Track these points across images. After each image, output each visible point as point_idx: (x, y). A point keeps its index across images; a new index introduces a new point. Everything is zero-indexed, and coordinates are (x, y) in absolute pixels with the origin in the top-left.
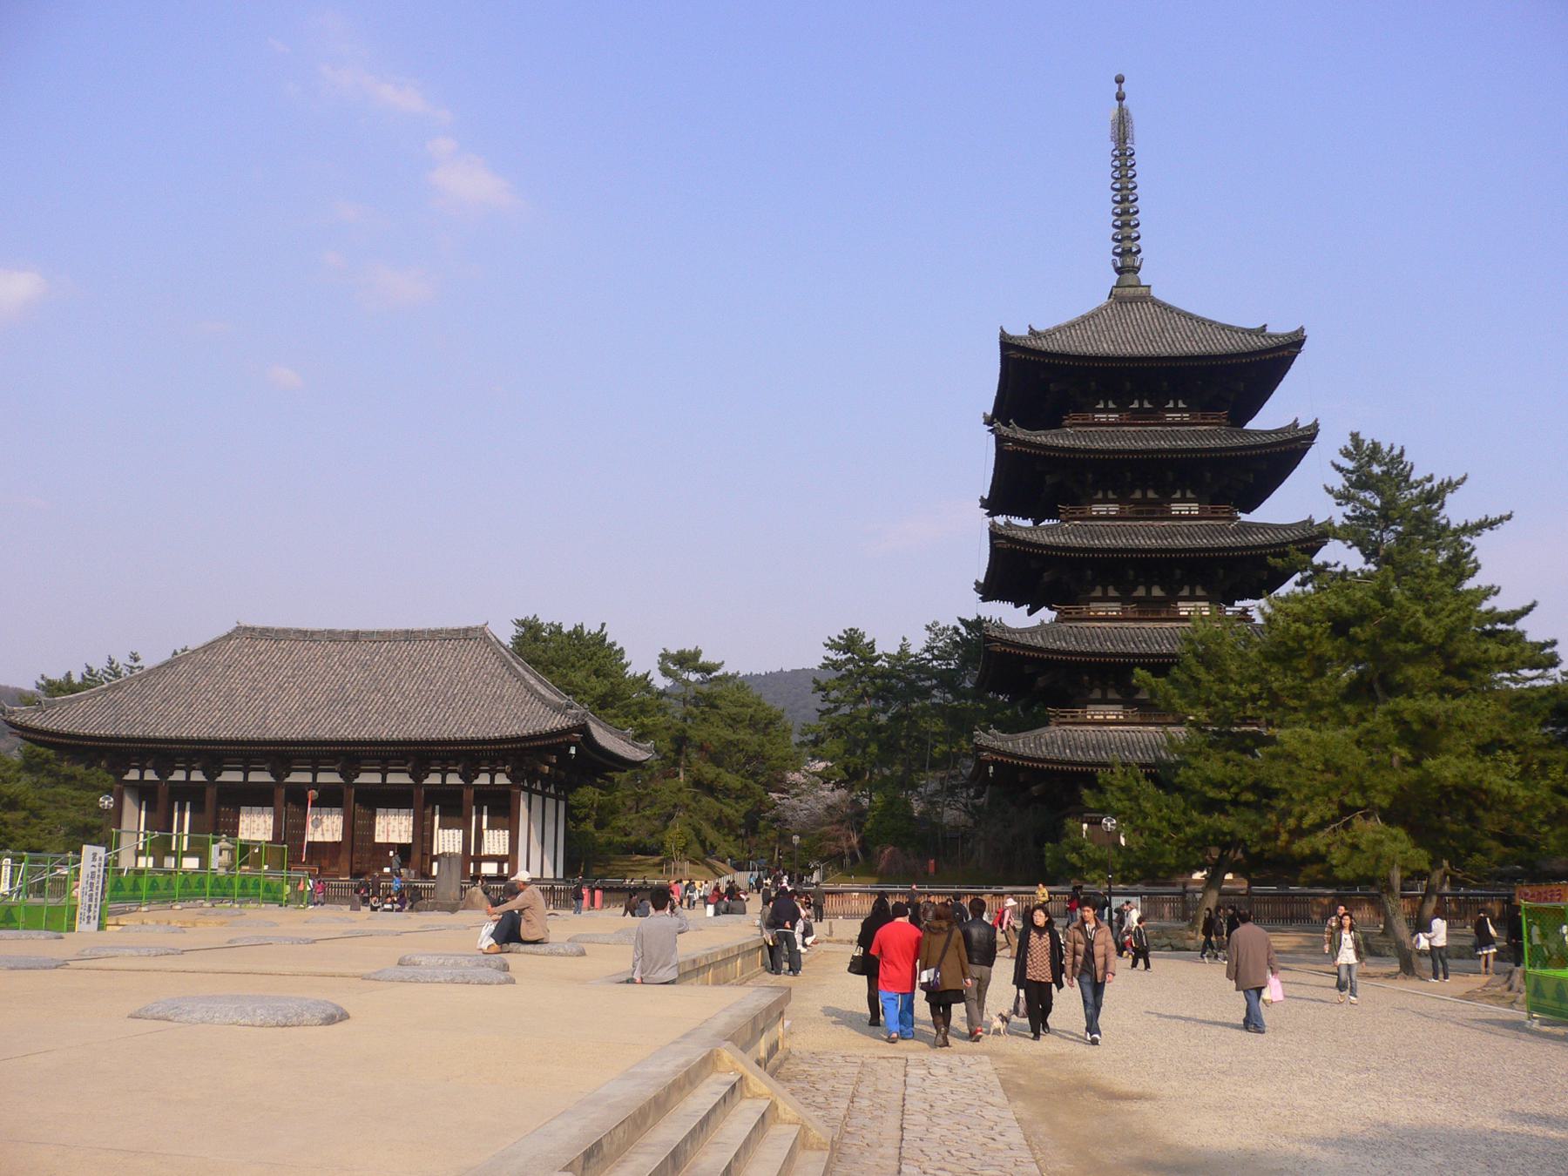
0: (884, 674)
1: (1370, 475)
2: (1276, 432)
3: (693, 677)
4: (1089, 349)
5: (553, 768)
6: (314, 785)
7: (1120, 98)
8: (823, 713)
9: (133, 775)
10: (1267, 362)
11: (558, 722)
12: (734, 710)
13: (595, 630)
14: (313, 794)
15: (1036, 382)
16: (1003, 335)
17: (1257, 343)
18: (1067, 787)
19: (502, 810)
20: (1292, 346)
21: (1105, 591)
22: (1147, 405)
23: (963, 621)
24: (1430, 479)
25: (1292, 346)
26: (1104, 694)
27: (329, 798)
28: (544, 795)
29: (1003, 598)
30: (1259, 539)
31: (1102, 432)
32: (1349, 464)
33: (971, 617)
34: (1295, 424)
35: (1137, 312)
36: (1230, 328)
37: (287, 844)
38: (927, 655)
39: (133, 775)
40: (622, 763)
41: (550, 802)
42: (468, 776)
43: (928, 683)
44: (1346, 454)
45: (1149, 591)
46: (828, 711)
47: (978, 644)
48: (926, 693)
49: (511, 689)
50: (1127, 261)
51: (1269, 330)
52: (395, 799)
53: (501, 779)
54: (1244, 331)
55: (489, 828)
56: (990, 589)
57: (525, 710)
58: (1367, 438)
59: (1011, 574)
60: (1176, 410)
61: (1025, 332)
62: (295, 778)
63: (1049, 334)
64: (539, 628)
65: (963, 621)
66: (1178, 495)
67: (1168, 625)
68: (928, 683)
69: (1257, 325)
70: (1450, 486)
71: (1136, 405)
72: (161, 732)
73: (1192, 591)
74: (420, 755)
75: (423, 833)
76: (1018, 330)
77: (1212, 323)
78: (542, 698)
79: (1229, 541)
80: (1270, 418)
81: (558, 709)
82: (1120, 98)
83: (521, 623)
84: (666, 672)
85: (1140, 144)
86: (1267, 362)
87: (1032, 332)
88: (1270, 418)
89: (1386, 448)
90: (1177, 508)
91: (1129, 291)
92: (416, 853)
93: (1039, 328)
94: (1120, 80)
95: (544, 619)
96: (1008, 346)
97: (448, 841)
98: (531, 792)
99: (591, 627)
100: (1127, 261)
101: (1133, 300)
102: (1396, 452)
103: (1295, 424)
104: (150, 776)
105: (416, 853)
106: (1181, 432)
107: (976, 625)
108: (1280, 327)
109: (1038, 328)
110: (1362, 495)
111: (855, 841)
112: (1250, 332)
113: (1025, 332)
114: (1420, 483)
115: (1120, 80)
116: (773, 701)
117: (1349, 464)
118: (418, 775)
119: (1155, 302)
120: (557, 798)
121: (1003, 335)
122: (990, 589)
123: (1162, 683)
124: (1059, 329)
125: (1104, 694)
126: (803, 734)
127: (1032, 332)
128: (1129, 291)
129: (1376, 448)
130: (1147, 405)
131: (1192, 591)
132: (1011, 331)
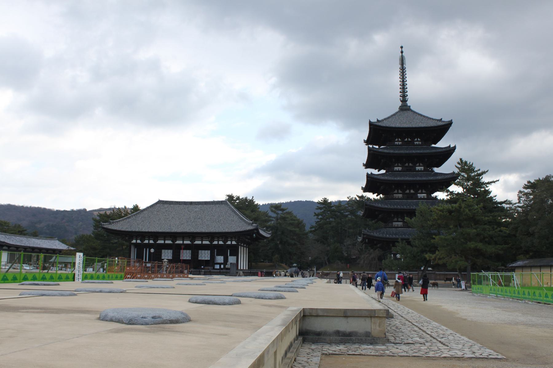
0: (334, 211)
1: (464, 169)
2: (445, 148)
3: (280, 212)
4: (393, 125)
5: (248, 238)
6: (183, 244)
7: (402, 52)
8: (317, 222)
9: (134, 241)
10: (442, 129)
11: (250, 228)
12: (291, 222)
13: (251, 198)
14: (183, 247)
15: (378, 134)
16: (370, 121)
17: (440, 124)
18: (387, 245)
19: (235, 252)
20: (450, 124)
21: (398, 191)
22: (409, 140)
23: (357, 196)
24: (479, 170)
25: (450, 124)
26: (398, 219)
27: (187, 247)
28: (244, 247)
29: (369, 191)
30: (440, 178)
31: (398, 147)
32: (459, 166)
33: (360, 195)
34: (450, 146)
35: (406, 113)
36: (432, 119)
37: (176, 259)
38: (347, 206)
39: (134, 241)
40: (265, 237)
41: (245, 248)
42: (225, 242)
43: (347, 213)
44: (459, 163)
45: (410, 191)
46: (318, 222)
47: (361, 203)
48: (347, 216)
49: (236, 218)
50: (404, 98)
51: (443, 120)
52: (204, 247)
53: (234, 243)
54: (436, 120)
55: (230, 255)
56: (365, 190)
57: (239, 224)
58: (464, 160)
59: (372, 184)
60: (417, 141)
61: (376, 121)
62: (178, 242)
63: (382, 120)
64: (233, 197)
65: (357, 196)
66: (418, 165)
67: (415, 201)
68: (347, 213)
69: (439, 118)
70: (484, 173)
71: (406, 140)
72: (143, 230)
73: (422, 191)
74: (211, 236)
75: (213, 257)
76: (374, 120)
77: (427, 117)
78: (244, 221)
79: (432, 178)
80: (442, 144)
81: (249, 224)
82: (402, 52)
83: (228, 196)
84: (272, 211)
85: (406, 66)
86: (442, 129)
87: (378, 120)
88: (442, 144)
89: (468, 163)
90: (417, 168)
91: (405, 107)
92: (211, 263)
93: (379, 119)
94: (402, 47)
95: (235, 194)
96: (371, 124)
97: (220, 259)
98: (241, 246)
99: (250, 198)
100: (404, 98)
101: (406, 110)
102: (471, 164)
103: (450, 146)
104: (139, 241)
105: (211, 263)
106: (417, 147)
107: (362, 197)
108: (446, 119)
109: (379, 119)
110: (462, 174)
111: (326, 258)
112: (438, 120)
113: (376, 121)
114: (477, 171)
115: (402, 47)
116: (299, 215)
117: (459, 166)
118: (211, 241)
119: (412, 111)
120: (246, 247)
121: (370, 121)
122: (366, 189)
123: (413, 210)
124: (385, 119)
125: (398, 219)
126: (311, 228)
127: (378, 120)
128: (405, 107)
129: (466, 162)
130: (409, 140)
131: (422, 191)
132: (372, 121)
